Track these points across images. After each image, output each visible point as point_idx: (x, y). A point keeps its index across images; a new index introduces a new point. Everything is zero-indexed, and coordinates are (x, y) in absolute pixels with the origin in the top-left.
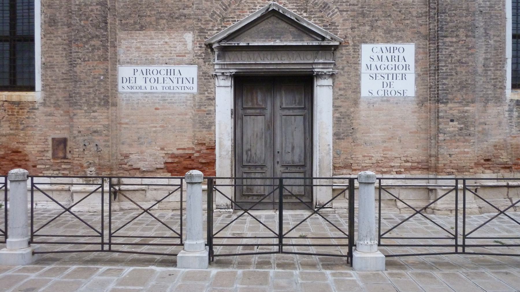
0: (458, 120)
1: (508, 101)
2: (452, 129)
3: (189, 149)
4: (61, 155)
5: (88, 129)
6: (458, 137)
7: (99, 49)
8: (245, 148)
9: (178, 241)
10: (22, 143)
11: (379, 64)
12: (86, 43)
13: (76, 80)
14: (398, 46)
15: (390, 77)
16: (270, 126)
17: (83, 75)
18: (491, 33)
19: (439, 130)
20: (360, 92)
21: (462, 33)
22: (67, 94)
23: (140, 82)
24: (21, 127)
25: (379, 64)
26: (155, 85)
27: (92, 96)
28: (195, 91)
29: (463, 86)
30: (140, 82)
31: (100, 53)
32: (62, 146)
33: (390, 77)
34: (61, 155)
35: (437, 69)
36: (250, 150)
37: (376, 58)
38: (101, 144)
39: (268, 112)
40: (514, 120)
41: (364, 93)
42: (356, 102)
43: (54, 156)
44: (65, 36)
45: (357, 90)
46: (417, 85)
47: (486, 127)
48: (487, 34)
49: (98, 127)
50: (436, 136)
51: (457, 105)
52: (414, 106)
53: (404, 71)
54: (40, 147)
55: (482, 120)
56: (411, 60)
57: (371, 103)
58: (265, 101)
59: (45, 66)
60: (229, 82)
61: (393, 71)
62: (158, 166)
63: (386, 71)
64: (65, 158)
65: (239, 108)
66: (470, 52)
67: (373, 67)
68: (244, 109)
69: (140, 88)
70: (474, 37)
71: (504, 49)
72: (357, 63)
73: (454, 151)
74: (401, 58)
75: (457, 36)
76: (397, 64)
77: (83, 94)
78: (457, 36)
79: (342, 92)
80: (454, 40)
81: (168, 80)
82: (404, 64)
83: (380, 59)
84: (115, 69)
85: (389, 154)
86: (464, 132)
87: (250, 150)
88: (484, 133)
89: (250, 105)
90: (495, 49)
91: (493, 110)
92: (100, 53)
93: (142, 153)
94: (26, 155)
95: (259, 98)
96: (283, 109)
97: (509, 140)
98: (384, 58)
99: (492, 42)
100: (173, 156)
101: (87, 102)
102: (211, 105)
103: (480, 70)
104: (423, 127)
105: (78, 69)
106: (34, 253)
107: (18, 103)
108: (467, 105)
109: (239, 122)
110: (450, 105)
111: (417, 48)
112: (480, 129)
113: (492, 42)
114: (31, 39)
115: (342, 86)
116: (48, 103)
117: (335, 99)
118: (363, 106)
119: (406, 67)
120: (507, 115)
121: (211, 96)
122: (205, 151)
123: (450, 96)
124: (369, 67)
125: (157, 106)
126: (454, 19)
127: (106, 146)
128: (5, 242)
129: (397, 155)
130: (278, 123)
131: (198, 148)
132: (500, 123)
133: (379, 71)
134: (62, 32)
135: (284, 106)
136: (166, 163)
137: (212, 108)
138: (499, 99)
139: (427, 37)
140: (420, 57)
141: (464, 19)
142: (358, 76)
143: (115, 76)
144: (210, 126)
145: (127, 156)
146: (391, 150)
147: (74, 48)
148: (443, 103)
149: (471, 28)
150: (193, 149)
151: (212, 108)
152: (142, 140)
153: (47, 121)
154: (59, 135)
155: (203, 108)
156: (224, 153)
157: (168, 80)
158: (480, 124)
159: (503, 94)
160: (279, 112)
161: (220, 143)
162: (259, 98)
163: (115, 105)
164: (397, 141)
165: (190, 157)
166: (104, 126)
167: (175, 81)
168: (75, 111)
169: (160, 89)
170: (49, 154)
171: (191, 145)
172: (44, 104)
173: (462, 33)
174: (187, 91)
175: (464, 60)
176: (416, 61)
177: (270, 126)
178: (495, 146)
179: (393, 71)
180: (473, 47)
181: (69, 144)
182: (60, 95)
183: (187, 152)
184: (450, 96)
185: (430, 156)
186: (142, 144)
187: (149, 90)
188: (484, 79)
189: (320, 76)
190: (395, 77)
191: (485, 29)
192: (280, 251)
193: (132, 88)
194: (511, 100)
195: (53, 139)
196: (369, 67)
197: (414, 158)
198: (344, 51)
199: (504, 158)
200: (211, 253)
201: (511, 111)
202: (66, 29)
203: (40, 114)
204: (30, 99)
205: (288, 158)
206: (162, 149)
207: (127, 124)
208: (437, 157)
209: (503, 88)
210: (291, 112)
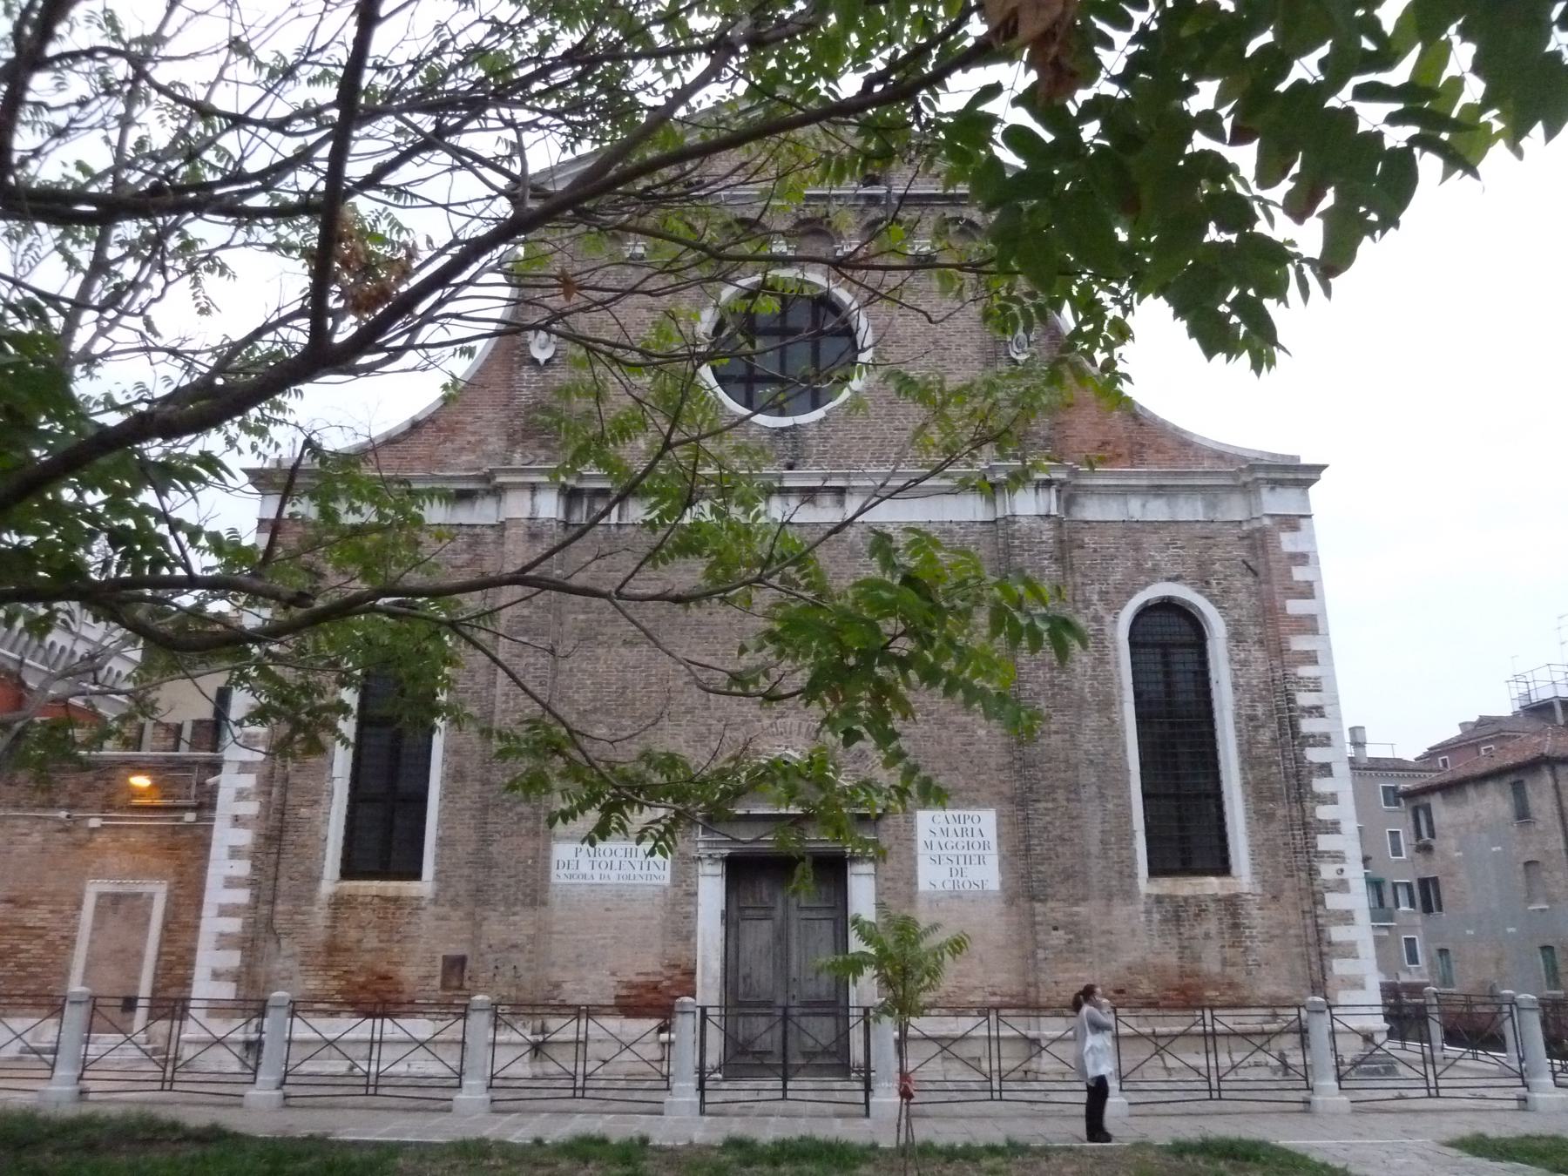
0: (1065, 927)
1: (1142, 897)
2: (1055, 942)
3: (654, 973)
4: (455, 983)
5: (503, 942)
6: (1066, 955)
7: (528, 819)
8: (741, 973)
9: (664, 1085)
10: (395, 963)
11: (943, 840)
12: (510, 809)
13: (489, 865)
14: (971, 813)
15: (962, 860)
16: (781, 937)
17: (501, 859)
18: (1109, 792)
19: (1038, 945)
20: (916, 884)
21: (1060, 795)
22: (473, 886)
23: (585, 868)
24: (396, 937)
25: (943, 840)
26: (608, 872)
27: (513, 890)
28: (667, 881)
29: (1068, 876)
30: (585, 868)
31: (530, 824)
32: (457, 970)
33: (962, 860)
34: (455, 983)
35: (1028, 849)
36: (749, 976)
37: (938, 831)
38: (522, 965)
39: (778, 913)
40: (1155, 926)
41: (923, 885)
42: (911, 899)
43: (444, 986)
44: (475, 797)
45: (912, 881)
46: (1002, 871)
47: (1113, 938)
48: (1102, 796)
49: (519, 938)
50: (1034, 954)
51: (1060, 904)
52: (998, 906)
53: (981, 852)
54: (422, 971)
55: (1104, 927)
56: (991, 834)
57: (934, 901)
58: (772, 896)
59: (442, 842)
60: (719, 869)
61: (965, 852)
62: (606, 1002)
63: (955, 851)
64: (461, 987)
65: (733, 906)
66: (1075, 823)
67: (935, 845)
68: (740, 909)
69: (585, 876)
70: (1079, 801)
71: (1129, 821)
72: (911, 840)
73: (1061, 976)
74: (976, 832)
75: (1054, 800)
76: (971, 840)
77: (499, 886)
78: (1054, 800)
79: (889, 884)
80: (1050, 805)
81: (626, 865)
82: (981, 840)
83: (945, 833)
84: (548, 849)
85: (967, 982)
86: (1074, 945)
87: (749, 976)
88: (1112, 948)
89: (750, 902)
90: (1117, 816)
91: (1120, 911)
92: (530, 824)
93: (581, 980)
94: (400, 983)
95: (765, 892)
96: (800, 908)
97: (1150, 958)
98: (951, 832)
99: (1110, 806)
100: (630, 985)
101: (505, 899)
102: (689, 904)
103: (1095, 849)
104: (1015, 938)
105: (493, 849)
106: (493, 1101)
107: (396, 900)
108: (1076, 904)
109: (732, 931)
110: (1051, 904)
111: (1000, 816)
112: (1103, 940)
113: (1110, 806)
114: (422, 800)
115: (890, 874)
116: (441, 901)
117: (879, 894)
118: (922, 905)
119: (985, 846)
120: (1143, 918)
121: (692, 889)
122: (679, 977)
123: (1049, 891)
124: (929, 845)
125: (608, 905)
126: (1048, 775)
127: (529, 969)
128: (460, 1086)
129: (977, 983)
130: (794, 931)
131: (668, 973)
132: (1133, 931)
133: (945, 851)
134: (472, 789)
135: (803, 904)
136: (617, 997)
137: (692, 909)
138: (1129, 894)
139: (1011, 800)
140: (1004, 830)
141: (1062, 775)
142: (913, 859)
143: (547, 858)
144: (687, 936)
145: (557, 986)
146: (967, 976)
147: (491, 817)
148: (1040, 901)
149: (1074, 790)
150: (661, 974)
151: (692, 909)
152: (583, 960)
153: (438, 928)
154: (454, 950)
155: (678, 908)
156: (709, 980)
157: (626, 865)
158: (1104, 932)
159: (1134, 885)
160: (794, 914)
161: (703, 966)
162: (765, 892)
163: (544, 903)
164: (976, 961)
165: (656, 988)
166: (528, 937)
167: (638, 866)
168: (486, 914)
169: (614, 880)
170: (437, 982)
171: (659, 968)
172: (435, 901)
173: (1060, 795)
174: (655, 881)
175: (1066, 836)
176: (999, 836)
177: (781, 937)
178: (1129, 968)
179: (965, 852)
180: (1078, 817)
181: (469, 964)
182: (462, 887)
183: (652, 978)
184: (1049, 891)
185: (1029, 985)
186: (583, 965)
187: (597, 880)
188: (1103, 862)
189: (855, 859)
190: (968, 860)
191: (1100, 788)
192: (784, 1098)
193: (572, 876)
194: (1148, 896)
195: (445, 958)
196: (929, 845)
197: (1005, 989)
198: (890, 821)
199: (1145, 988)
200: (702, 1102)
201: (1148, 912)
202: (478, 787)
203: (426, 919)
204: (414, 893)
205: (811, 990)
206: (613, 974)
207: (561, 933)
208: (1036, 985)
209: (1133, 876)
210: (813, 915)
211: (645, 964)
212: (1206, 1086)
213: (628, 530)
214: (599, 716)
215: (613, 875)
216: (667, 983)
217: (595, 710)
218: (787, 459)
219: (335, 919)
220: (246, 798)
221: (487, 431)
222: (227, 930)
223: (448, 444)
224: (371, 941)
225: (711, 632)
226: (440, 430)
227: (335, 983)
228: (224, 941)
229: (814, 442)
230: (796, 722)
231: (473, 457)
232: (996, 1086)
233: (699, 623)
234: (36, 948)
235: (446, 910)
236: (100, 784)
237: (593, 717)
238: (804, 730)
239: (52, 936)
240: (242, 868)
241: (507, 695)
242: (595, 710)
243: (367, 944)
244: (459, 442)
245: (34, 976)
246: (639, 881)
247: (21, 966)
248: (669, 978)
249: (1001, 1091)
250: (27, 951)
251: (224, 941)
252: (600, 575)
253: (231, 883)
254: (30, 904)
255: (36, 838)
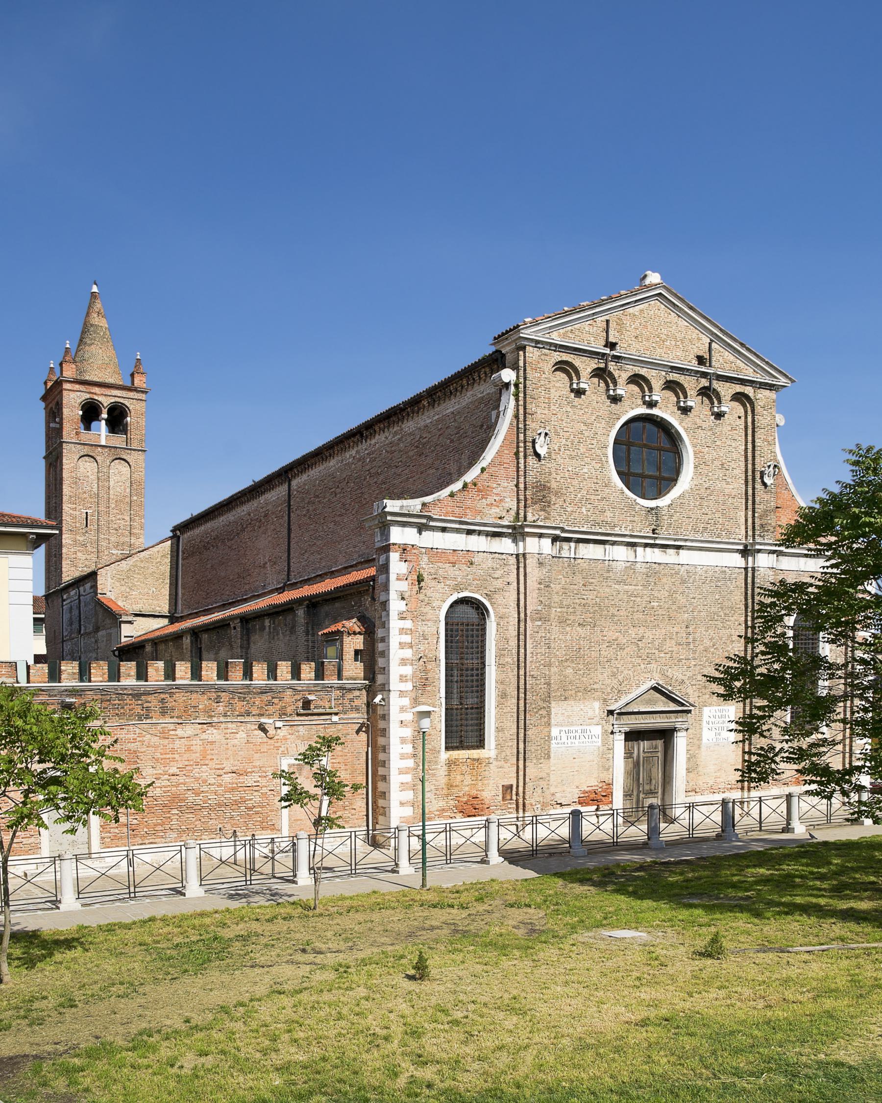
3: (595, 786)
10: (480, 790)
12: (537, 712)
24: (480, 778)
26: (574, 741)
28: (600, 744)
31: (546, 720)
32: (509, 790)
45: (700, 739)
54: (493, 793)
60: (623, 737)
61: (722, 725)
63: (718, 725)
67: (710, 723)
76: (724, 719)
81: (582, 737)
83: (715, 717)
116: (499, 759)
122: (605, 787)
131: (600, 785)
144: (608, 769)
150: (597, 786)
152: (564, 782)
157: (582, 737)
167: (587, 737)
170: (500, 797)
171: (596, 784)
172: (496, 759)
174: (594, 744)
179: (722, 725)
183: (594, 788)
211: (590, 782)
212: (349, 868)
213: (579, 561)
214: (568, 663)
215: (577, 741)
216: (600, 790)
217: (567, 660)
218: (653, 527)
219: (449, 771)
220: (405, 711)
221: (505, 494)
222: (404, 781)
223: (484, 500)
224: (468, 780)
225: (619, 620)
226: (479, 491)
227: (452, 802)
228: (403, 786)
229: (665, 518)
230: (655, 666)
231: (498, 511)
232: (132, 890)
233: (613, 615)
234: (256, 798)
235: (502, 763)
236: (276, 701)
237: (566, 664)
238: (658, 670)
239: (264, 790)
240: (408, 749)
241: (532, 653)
242: (567, 660)
243: (466, 783)
244: (490, 500)
245: (257, 813)
246: (588, 744)
247: (248, 808)
248: (600, 788)
249: (251, 880)
250: (251, 800)
251: (403, 786)
252: (567, 586)
253: (403, 757)
254: (246, 773)
255: (242, 735)
